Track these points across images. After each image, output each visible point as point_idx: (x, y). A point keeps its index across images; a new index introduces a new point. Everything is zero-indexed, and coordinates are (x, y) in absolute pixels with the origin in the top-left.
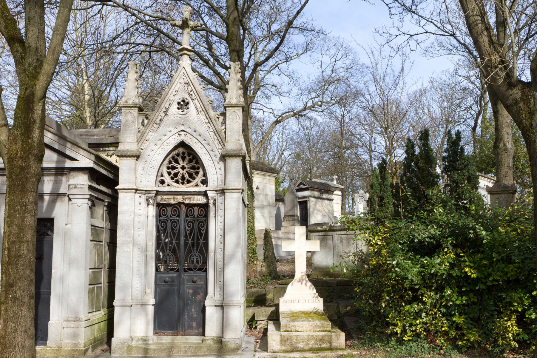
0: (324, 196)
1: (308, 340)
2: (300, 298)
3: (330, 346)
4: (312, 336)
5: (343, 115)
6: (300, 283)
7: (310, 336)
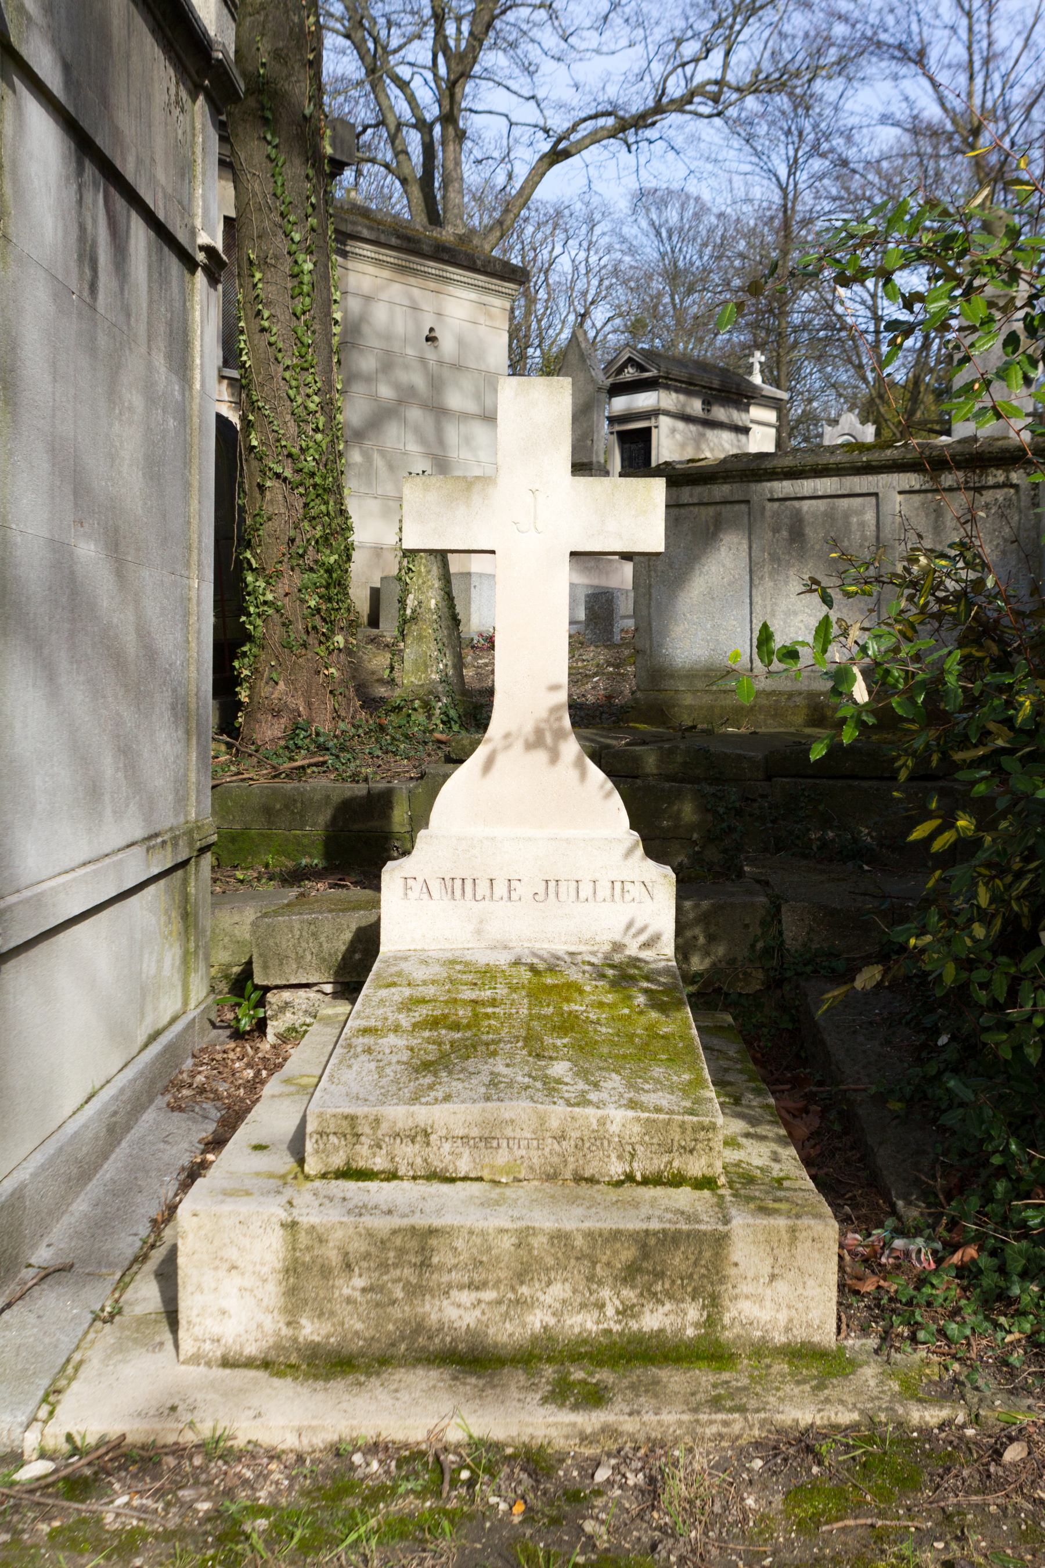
0: (720, 413)
1: (522, 1275)
2: (533, 861)
3: (711, 1322)
4: (560, 1237)
5: (796, 160)
6: (541, 756)
7: (539, 1242)
